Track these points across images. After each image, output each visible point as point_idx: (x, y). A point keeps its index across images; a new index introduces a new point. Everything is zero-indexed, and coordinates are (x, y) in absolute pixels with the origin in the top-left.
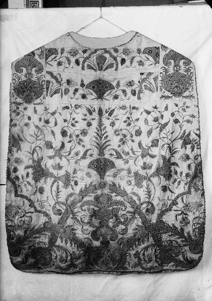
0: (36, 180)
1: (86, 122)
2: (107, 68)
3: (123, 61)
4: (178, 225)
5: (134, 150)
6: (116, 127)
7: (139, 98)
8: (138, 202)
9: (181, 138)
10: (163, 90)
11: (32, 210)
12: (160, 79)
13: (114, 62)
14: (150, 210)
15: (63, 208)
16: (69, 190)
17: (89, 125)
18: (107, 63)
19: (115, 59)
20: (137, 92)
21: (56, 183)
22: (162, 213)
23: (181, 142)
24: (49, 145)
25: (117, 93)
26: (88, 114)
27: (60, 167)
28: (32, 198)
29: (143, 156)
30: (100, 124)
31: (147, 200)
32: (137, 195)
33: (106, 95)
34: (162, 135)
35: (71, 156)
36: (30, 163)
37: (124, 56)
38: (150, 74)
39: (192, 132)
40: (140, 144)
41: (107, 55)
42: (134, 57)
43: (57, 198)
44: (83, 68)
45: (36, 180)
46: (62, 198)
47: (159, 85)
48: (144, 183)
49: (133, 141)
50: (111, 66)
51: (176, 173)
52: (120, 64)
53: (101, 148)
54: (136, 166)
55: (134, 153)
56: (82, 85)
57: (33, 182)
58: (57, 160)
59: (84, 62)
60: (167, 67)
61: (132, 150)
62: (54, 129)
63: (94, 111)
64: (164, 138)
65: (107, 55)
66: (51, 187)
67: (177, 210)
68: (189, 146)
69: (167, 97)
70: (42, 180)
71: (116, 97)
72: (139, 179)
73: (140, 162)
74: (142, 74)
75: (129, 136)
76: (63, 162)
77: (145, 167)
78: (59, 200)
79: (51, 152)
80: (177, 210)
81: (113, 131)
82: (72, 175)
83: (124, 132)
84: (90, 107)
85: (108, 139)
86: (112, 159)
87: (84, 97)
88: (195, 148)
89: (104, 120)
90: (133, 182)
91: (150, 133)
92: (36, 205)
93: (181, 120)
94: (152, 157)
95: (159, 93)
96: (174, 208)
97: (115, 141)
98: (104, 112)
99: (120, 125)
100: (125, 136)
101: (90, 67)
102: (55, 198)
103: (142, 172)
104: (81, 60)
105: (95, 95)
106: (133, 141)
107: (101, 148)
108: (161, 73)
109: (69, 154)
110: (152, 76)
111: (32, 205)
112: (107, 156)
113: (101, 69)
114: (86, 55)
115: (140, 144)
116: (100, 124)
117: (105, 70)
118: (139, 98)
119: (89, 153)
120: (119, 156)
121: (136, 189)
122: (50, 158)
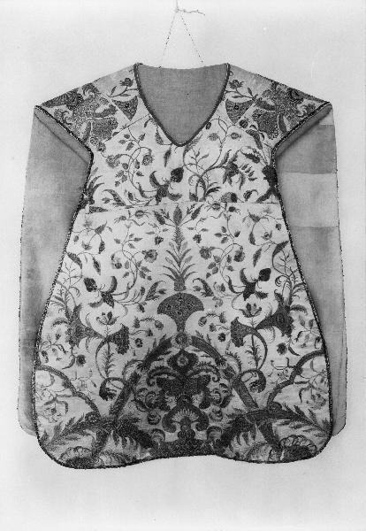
0: (73, 342)
1: (152, 237)
5: (233, 284)
6: (203, 244)
8: (237, 370)
11: (68, 392)
14: (261, 384)
15: (116, 387)
16: (129, 356)
17: (158, 240)
21: (106, 346)
22: (278, 389)
23: (221, 172)
24: (90, 285)
26: (158, 223)
27: (110, 319)
28: (66, 372)
30: (178, 238)
31: (253, 367)
32: (235, 357)
34: (188, 159)
35: (129, 299)
36: (62, 315)
40: (153, 179)
43: (107, 373)
45: (73, 342)
46: (116, 371)
48: (247, 339)
49: (230, 269)
53: (179, 279)
54: (233, 309)
55: (231, 288)
57: (67, 347)
58: (105, 308)
61: (230, 283)
62: (99, 258)
63: (168, 217)
64: (191, 164)
66: (98, 350)
67: (301, 382)
68: (236, 178)
70: (83, 342)
72: (238, 333)
73: (241, 303)
75: (132, 168)
76: (117, 311)
77: (249, 311)
78: (111, 375)
79: (95, 296)
80: (301, 382)
81: (104, 159)
82: (131, 330)
83: (124, 160)
84: (160, 212)
85: (191, 262)
86: (198, 295)
88: (247, 179)
89: (184, 229)
90: (228, 338)
92: (75, 383)
93: (222, 135)
94: (262, 296)
96: (298, 379)
97: (199, 267)
98: (184, 213)
99: (209, 240)
100: (218, 260)
102: (103, 372)
103: (245, 321)
106: (230, 269)
107: (179, 279)
109: (127, 296)
111: (67, 384)
112: (189, 292)
115: (153, 179)
116: (178, 238)
119: (158, 289)
120: (208, 293)
121: (234, 349)
122: (93, 305)
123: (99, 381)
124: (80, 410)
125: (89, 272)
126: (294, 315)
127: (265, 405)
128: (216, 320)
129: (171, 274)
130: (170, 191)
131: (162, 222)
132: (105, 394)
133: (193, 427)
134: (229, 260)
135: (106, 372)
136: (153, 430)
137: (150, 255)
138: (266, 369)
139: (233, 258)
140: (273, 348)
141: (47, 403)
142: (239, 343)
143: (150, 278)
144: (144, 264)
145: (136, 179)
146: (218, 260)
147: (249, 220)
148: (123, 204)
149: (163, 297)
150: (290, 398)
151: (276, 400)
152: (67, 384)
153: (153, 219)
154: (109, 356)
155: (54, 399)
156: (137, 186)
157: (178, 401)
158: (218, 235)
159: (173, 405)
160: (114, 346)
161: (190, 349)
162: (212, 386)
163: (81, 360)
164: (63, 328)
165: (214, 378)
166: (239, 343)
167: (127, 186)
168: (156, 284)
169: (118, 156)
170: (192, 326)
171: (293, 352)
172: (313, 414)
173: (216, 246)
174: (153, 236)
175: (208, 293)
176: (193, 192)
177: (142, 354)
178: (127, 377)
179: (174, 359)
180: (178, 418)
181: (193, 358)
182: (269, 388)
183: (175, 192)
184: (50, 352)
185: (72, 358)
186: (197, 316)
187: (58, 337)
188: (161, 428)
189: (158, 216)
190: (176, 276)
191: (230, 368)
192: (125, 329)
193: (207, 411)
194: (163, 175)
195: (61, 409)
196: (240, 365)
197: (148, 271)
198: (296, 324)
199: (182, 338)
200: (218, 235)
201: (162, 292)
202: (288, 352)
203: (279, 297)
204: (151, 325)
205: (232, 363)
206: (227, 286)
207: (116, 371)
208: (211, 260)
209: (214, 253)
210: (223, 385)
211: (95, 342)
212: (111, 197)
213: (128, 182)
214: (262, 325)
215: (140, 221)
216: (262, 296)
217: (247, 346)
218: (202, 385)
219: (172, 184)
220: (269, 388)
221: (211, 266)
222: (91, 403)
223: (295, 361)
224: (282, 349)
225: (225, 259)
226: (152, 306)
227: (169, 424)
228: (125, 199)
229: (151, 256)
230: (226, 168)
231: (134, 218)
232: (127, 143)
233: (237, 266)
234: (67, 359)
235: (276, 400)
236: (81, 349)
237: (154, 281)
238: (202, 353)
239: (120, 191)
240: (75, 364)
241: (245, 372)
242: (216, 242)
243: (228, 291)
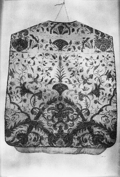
0: (22, 94)
2: (64, 33)
3: (73, 30)
4: (103, 123)
6: (69, 67)
7: (82, 51)
8: (80, 109)
9: (106, 75)
10: (96, 48)
11: (19, 111)
12: (94, 41)
13: (68, 30)
14: (88, 113)
18: (64, 30)
19: (69, 29)
20: (81, 48)
21: (33, 97)
25: (70, 47)
26: (53, 59)
29: (84, 83)
31: (86, 108)
33: (63, 48)
37: (73, 27)
38: (88, 39)
39: (112, 71)
41: (64, 26)
42: (79, 29)
44: (51, 33)
45: (22, 94)
46: (37, 106)
47: (94, 45)
48: (84, 98)
50: (66, 32)
51: (103, 94)
52: (71, 32)
53: (60, 79)
56: (51, 43)
57: (20, 96)
59: (51, 29)
60: (97, 35)
61: (78, 80)
63: (57, 57)
65: (64, 26)
67: (102, 114)
68: (110, 79)
69: (98, 52)
71: (69, 50)
73: (82, 86)
74: (84, 38)
78: (35, 106)
80: (102, 114)
84: (54, 55)
86: (67, 84)
87: (51, 49)
90: (78, 98)
91: (88, 71)
92: (22, 108)
95: (94, 50)
101: (54, 32)
103: (83, 92)
104: (50, 29)
105: (57, 48)
107: (60, 79)
108: (94, 38)
110: (89, 40)
111: (19, 108)
112: (64, 83)
113: (61, 33)
114: (52, 26)
115: (82, 76)
117: (63, 34)
118: (82, 51)
119: (53, 81)
123: (31, 108)
124: (22, 118)
125: (30, 72)
126: (101, 91)
127: (90, 120)
128: (73, 92)
129: (58, 77)
130: (88, 82)
131: (55, 58)
132: (32, 112)
133: (63, 129)
134: (78, 72)
135: (34, 104)
136: (49, 128)
137: (50, 69)
138: (90, 109)
139: (79, 71)
140: (93, 101)
141: (13, 115)
142: (81, 100)
143: (50, 77)
144: (48, 71)
145: (77, 76)
146: (74, 72)
147: (85, 60)
148: (72, 84)
149: (55, 84)
150: (98, 119)
151: (93, 119)
152: (19, 108)
153: (52, 57)
154: (35, 100)
155: (15, 114)
156: (77, 79)
157: (59, 119)
158: (74, 64)
159: (56, 121)
160: (37, 97)
161: (62, 102)
162: (70, 115)
163: (25, 101)
164: (19, 89)
165: (71, 112)
166: (81, 100)
167: (74, 78)
168: (52, 79)
169: (72, 68)
170: (65, 94)
171: (99, 103)
172: (105, 125)
173: (73, 67)
174: (52, 63)
175: (70, 83)
176: (96, 83)
177: (46, 101)
178: (41, 108)
179: (58, 105)
180: (58, 125)
181: (63, 106)
182: (91, 115)
183: (89, 82)
184: (14, 98)
185: (21, 100)
186: (66, 91)
187: (17, 92)
188: (52, 128)
189: (53, 57)
190: (59, 77)
191: (78, 108)
192: (41, 92)
193: (68, 123)
194: (86, 75)
195: (16, 117)
196: (81, 107)
197: (50, 74)
198: (101, 94)
199: (60, 98)
200: (74, 64)
201: (54, 82)
202: (98, 103)
203: (96, 85)
204: (49, 92)
205: (78, 106)
206: (77, 80)
207: (37, 106)
208: (72, 72)
209: (73, 70)
210: (75, 114)
211: (30, 96)
212: (68, 81)
213: (74, 77)
214: (89, 94)
215: (47, 57)
216: (89, 84)
217: (84, 101)
218: (67, 115)
219: (89, 79)
220: (91, 115)
221: (72, 74)
222: (28, 115)
223: (100, 107)
224: (96, 102)
225: (76, 72)
226: (51, 86)
227: (54, 126)
228: (73, 82)
229: (51, 69)
230: (108, 75)
231: (45, 56)
232: (75, 65)
233: (81, 74)
234: (20, 100)
235: (93, 119)
236: (25, 97)
237: (52, 78)
238: (67, 104)
239: (71, 79)
240: (22, 102)
241: (83, 109)
242: (74, 66)
243: (77, 82)
